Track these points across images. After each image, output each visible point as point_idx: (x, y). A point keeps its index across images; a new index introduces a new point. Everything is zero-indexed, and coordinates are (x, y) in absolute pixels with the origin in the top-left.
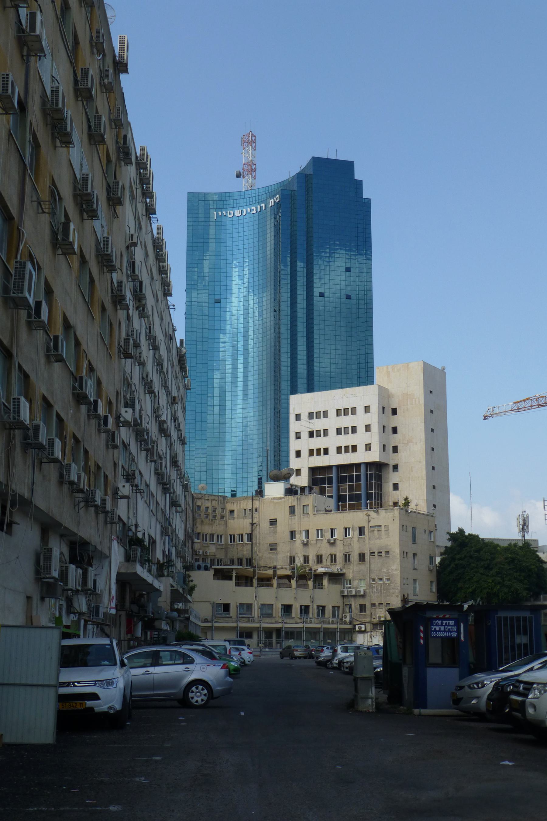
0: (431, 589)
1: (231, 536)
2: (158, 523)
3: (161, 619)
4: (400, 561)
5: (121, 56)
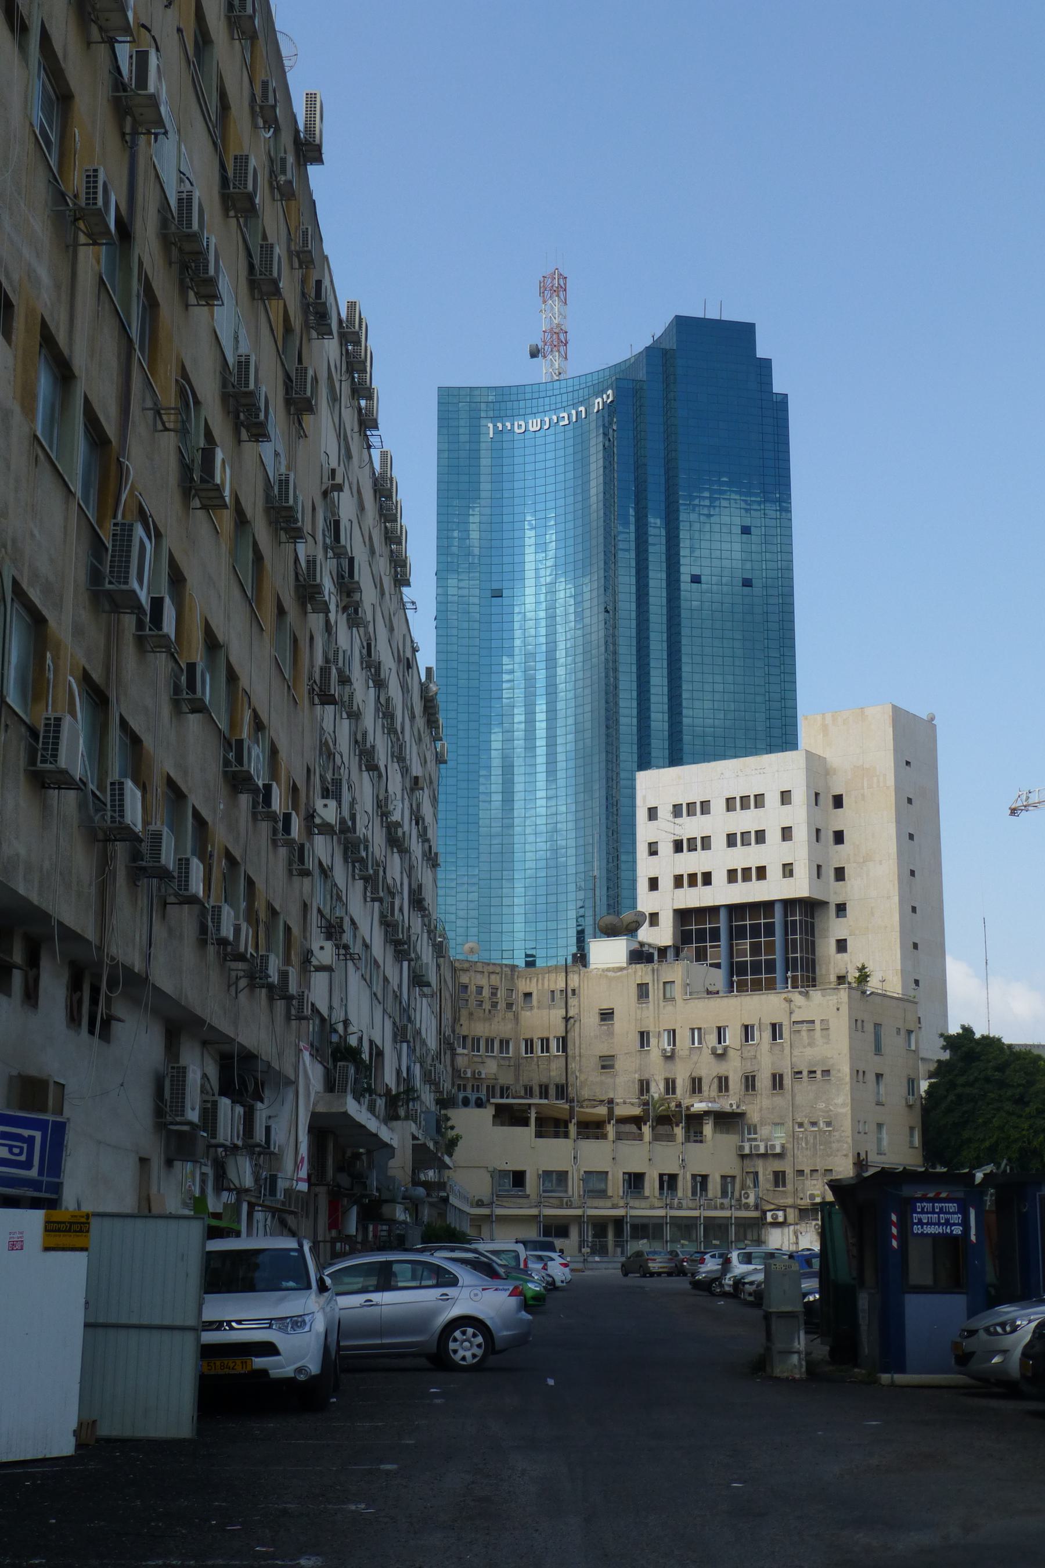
0: (911, 1142)
1: (526, 1041)
2: (386, 1017)
3: (392, 1201)
4: (852, 1089)
5: (310, 128)
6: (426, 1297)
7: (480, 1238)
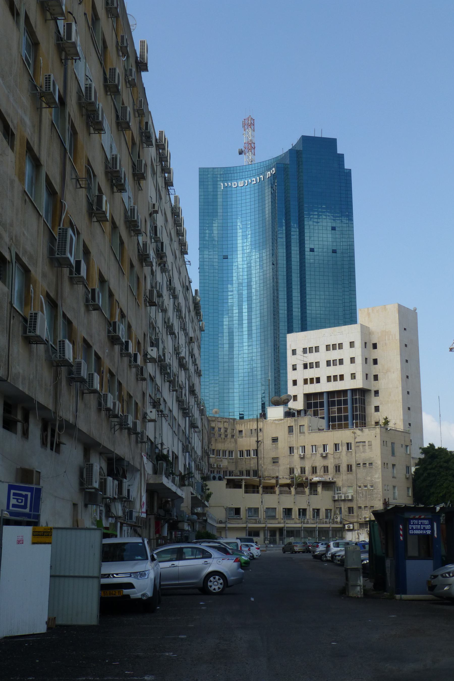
0: (408, 494)
2: (179, 442)
3: (183, 521)
4: (382, 471)
6: (198, 563)
7: (221, 537)
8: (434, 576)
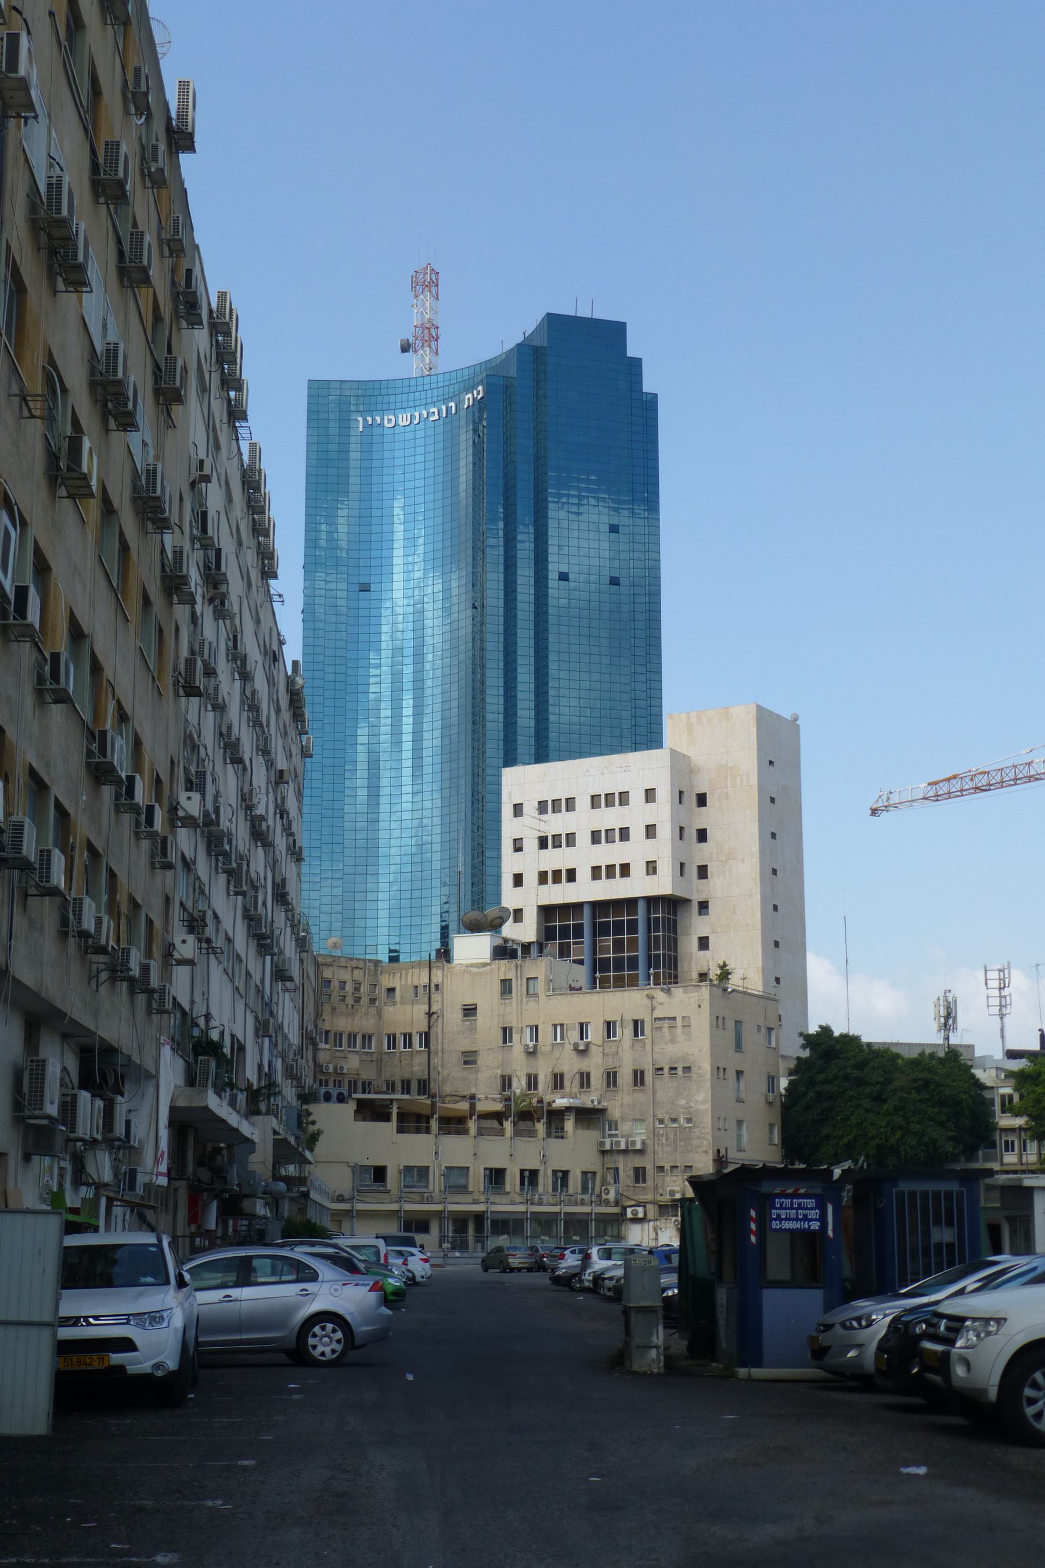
0: (771, 1139)
2: (248, 1012)
3: (253, 1196)
4: (712, 1085)
7: (340, 1234)
8: (824, 1326)
